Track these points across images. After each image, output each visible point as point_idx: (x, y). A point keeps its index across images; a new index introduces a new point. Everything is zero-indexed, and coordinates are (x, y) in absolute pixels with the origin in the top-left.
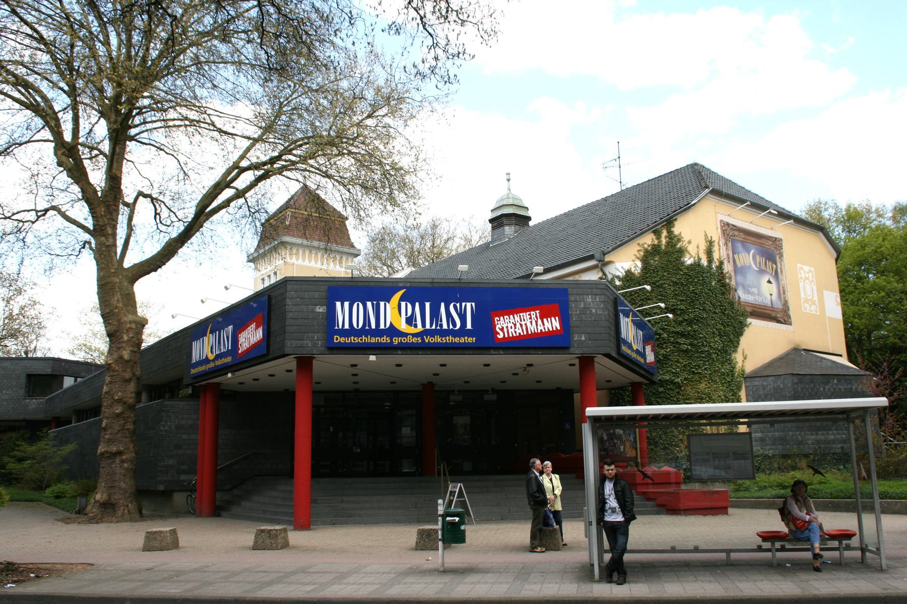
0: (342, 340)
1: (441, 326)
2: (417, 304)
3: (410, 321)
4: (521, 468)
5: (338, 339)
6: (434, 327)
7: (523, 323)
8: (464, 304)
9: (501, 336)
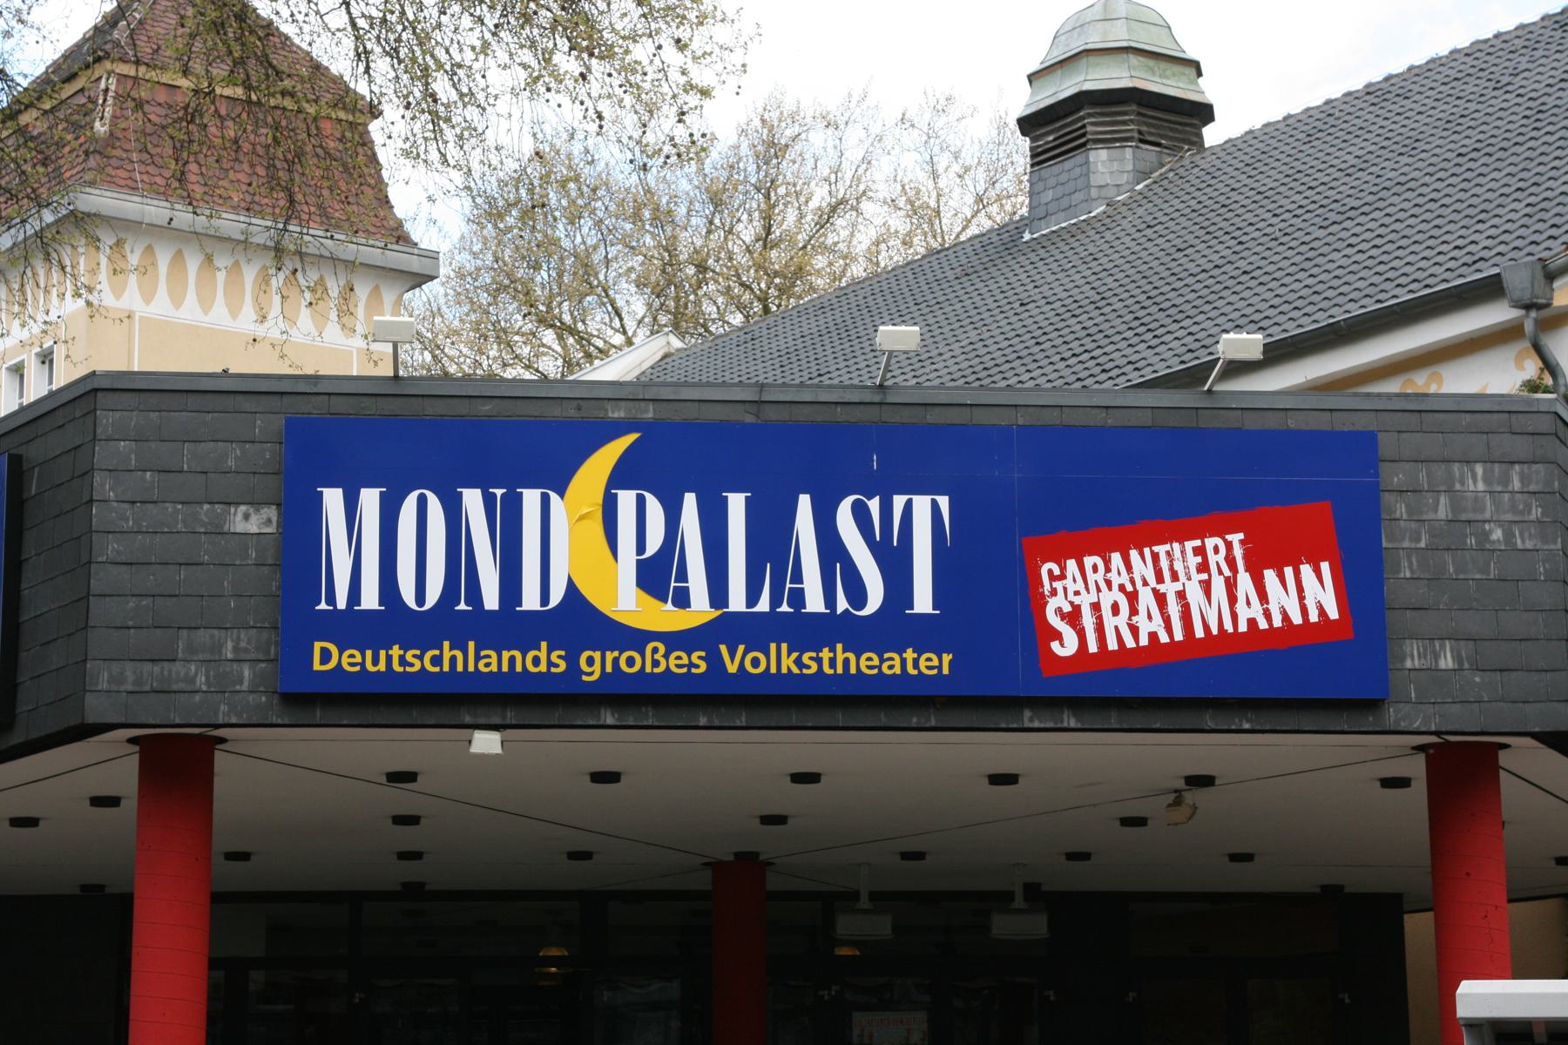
0: (349, 660)
5: (331, 658)
7: (1169, 588)
9: (1066, 647)
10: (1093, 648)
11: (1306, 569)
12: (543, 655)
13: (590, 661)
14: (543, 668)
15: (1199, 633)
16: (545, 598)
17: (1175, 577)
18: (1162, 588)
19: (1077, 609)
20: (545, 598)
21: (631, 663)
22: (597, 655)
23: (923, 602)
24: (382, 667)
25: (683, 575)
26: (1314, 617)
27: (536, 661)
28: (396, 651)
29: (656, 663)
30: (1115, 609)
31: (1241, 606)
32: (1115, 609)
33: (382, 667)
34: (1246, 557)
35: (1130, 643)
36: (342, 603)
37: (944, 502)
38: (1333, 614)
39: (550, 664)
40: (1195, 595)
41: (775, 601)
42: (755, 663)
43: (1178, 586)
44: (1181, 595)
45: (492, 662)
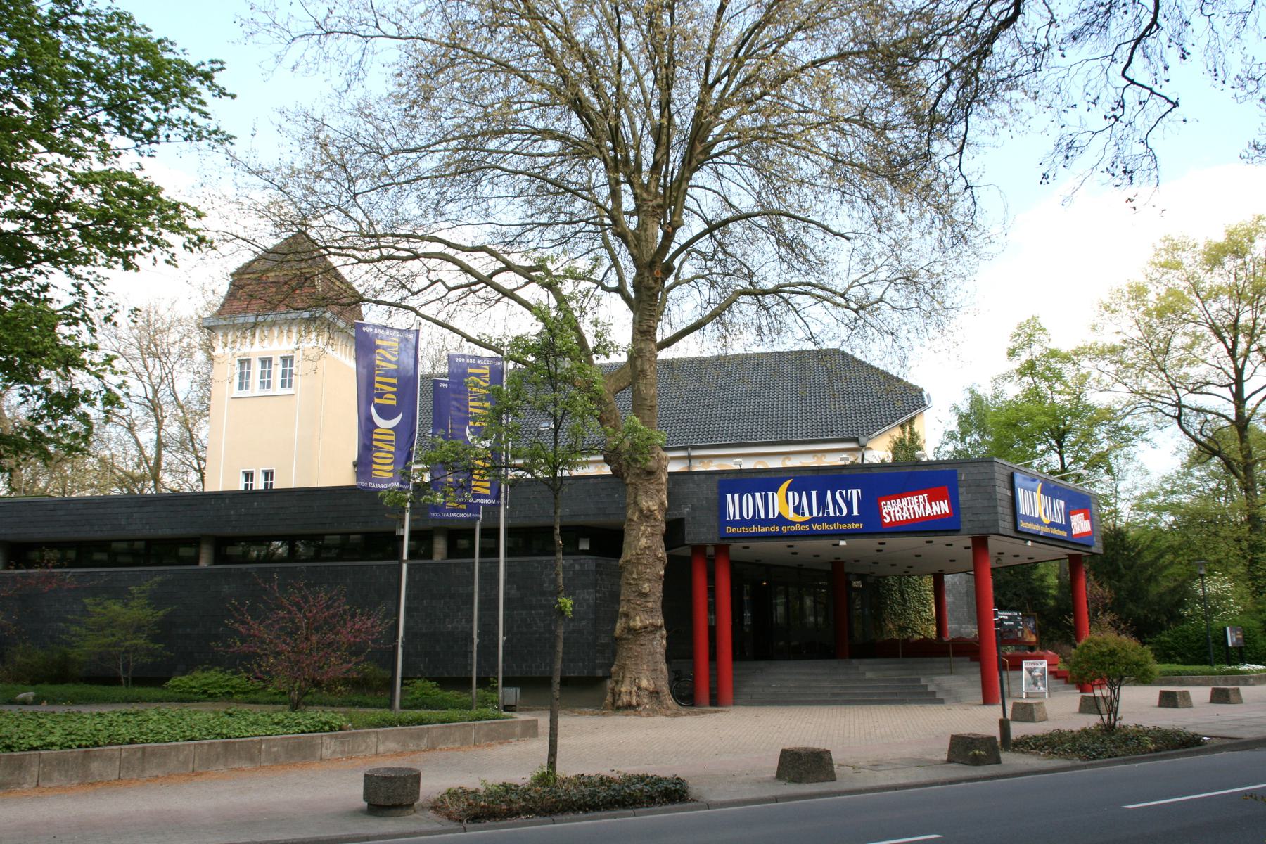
0: (734, 530)
3: (797, 510)
21: (793, 528)
23: (856, 512)
45: (763, 530)
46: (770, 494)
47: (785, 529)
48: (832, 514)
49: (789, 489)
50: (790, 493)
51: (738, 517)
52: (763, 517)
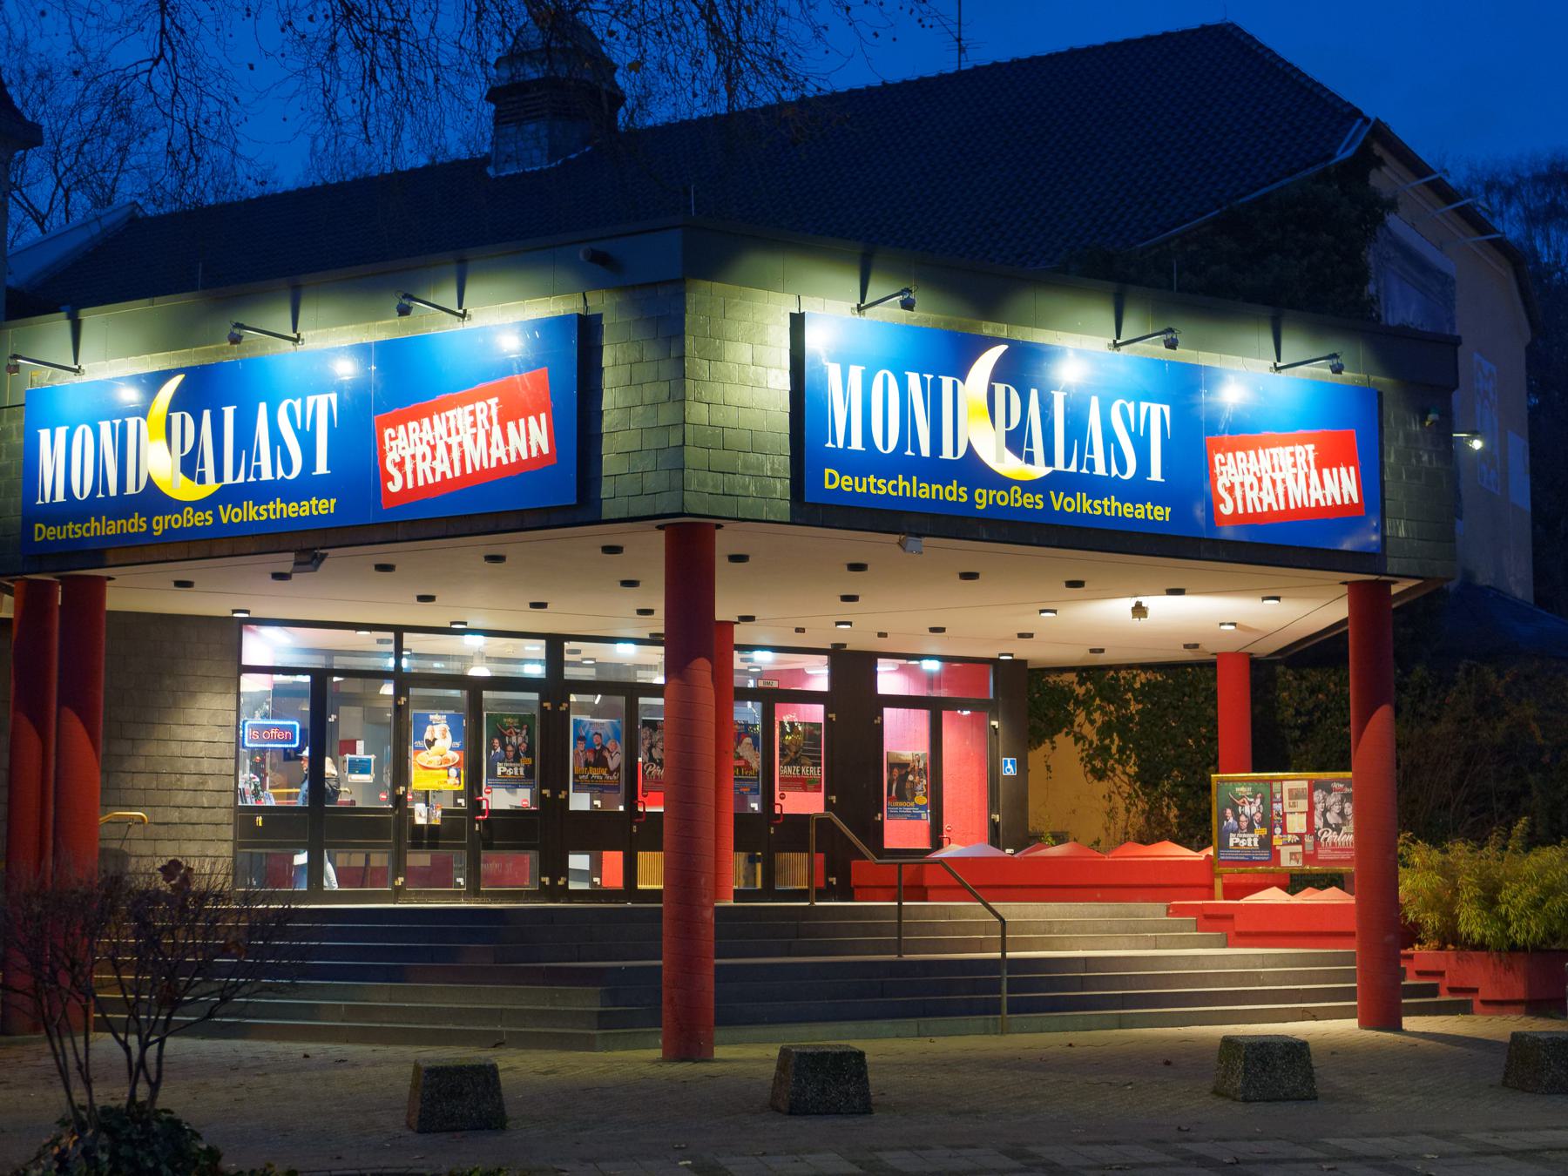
0: (845, 482)
1: (258, 471)
2: (207, 414)
3: (190, 465)
4: (1405, 829)
5: (837, 481)
6: (241, 479)
7: (454, 441)
8: (310, 400)
9: (394, 487)
10: (1241, 511)
11: (1343, 470)
12: (954, 489)
13: (981, 496)
14: (954, 498)
15: (1292, 506)
16: (955, 453)
17: (458, 432)
18: (450, 441)
19: (403, 459)
20: (955, 453)
21: (1004, 499)
22: (984, 492)
23: (1156, 474)
24: (864, 490)
25: (1030, 445)
26: (1347, 501)
27: (951, 493)
28: (872, 479)
29: (1016, 501)
30: (424, 458)
31: (1312, 490)
32: (424, 458)
33: (864, 490)
34: (499, 414)
35: (1259, 510)
36: (840, 445)
37: (1167, 409)
38: (1356, 500)
39: (959, 496)
40: (1291, 484)
41: (1080, 466)
42: (1069, 504)
43: (458, 439)
44: (1284, 481)
45: (926, 491)
46: (947, 382)
47: (160, 524)
48: (1100, 470)
49: (175, 405)
50: (176, 417)
51: (857, 444)
52: (925, 451)
